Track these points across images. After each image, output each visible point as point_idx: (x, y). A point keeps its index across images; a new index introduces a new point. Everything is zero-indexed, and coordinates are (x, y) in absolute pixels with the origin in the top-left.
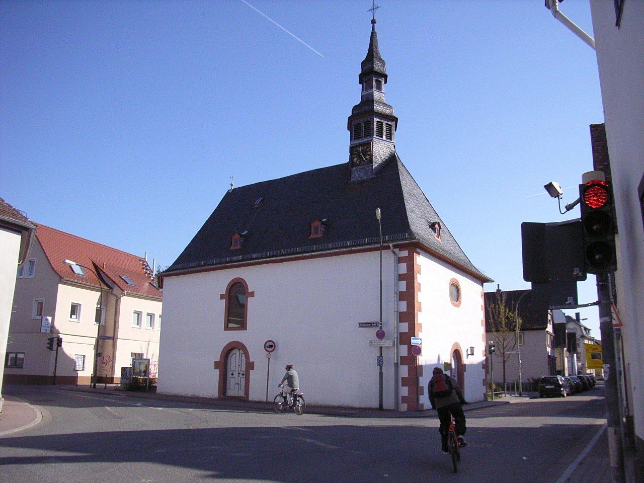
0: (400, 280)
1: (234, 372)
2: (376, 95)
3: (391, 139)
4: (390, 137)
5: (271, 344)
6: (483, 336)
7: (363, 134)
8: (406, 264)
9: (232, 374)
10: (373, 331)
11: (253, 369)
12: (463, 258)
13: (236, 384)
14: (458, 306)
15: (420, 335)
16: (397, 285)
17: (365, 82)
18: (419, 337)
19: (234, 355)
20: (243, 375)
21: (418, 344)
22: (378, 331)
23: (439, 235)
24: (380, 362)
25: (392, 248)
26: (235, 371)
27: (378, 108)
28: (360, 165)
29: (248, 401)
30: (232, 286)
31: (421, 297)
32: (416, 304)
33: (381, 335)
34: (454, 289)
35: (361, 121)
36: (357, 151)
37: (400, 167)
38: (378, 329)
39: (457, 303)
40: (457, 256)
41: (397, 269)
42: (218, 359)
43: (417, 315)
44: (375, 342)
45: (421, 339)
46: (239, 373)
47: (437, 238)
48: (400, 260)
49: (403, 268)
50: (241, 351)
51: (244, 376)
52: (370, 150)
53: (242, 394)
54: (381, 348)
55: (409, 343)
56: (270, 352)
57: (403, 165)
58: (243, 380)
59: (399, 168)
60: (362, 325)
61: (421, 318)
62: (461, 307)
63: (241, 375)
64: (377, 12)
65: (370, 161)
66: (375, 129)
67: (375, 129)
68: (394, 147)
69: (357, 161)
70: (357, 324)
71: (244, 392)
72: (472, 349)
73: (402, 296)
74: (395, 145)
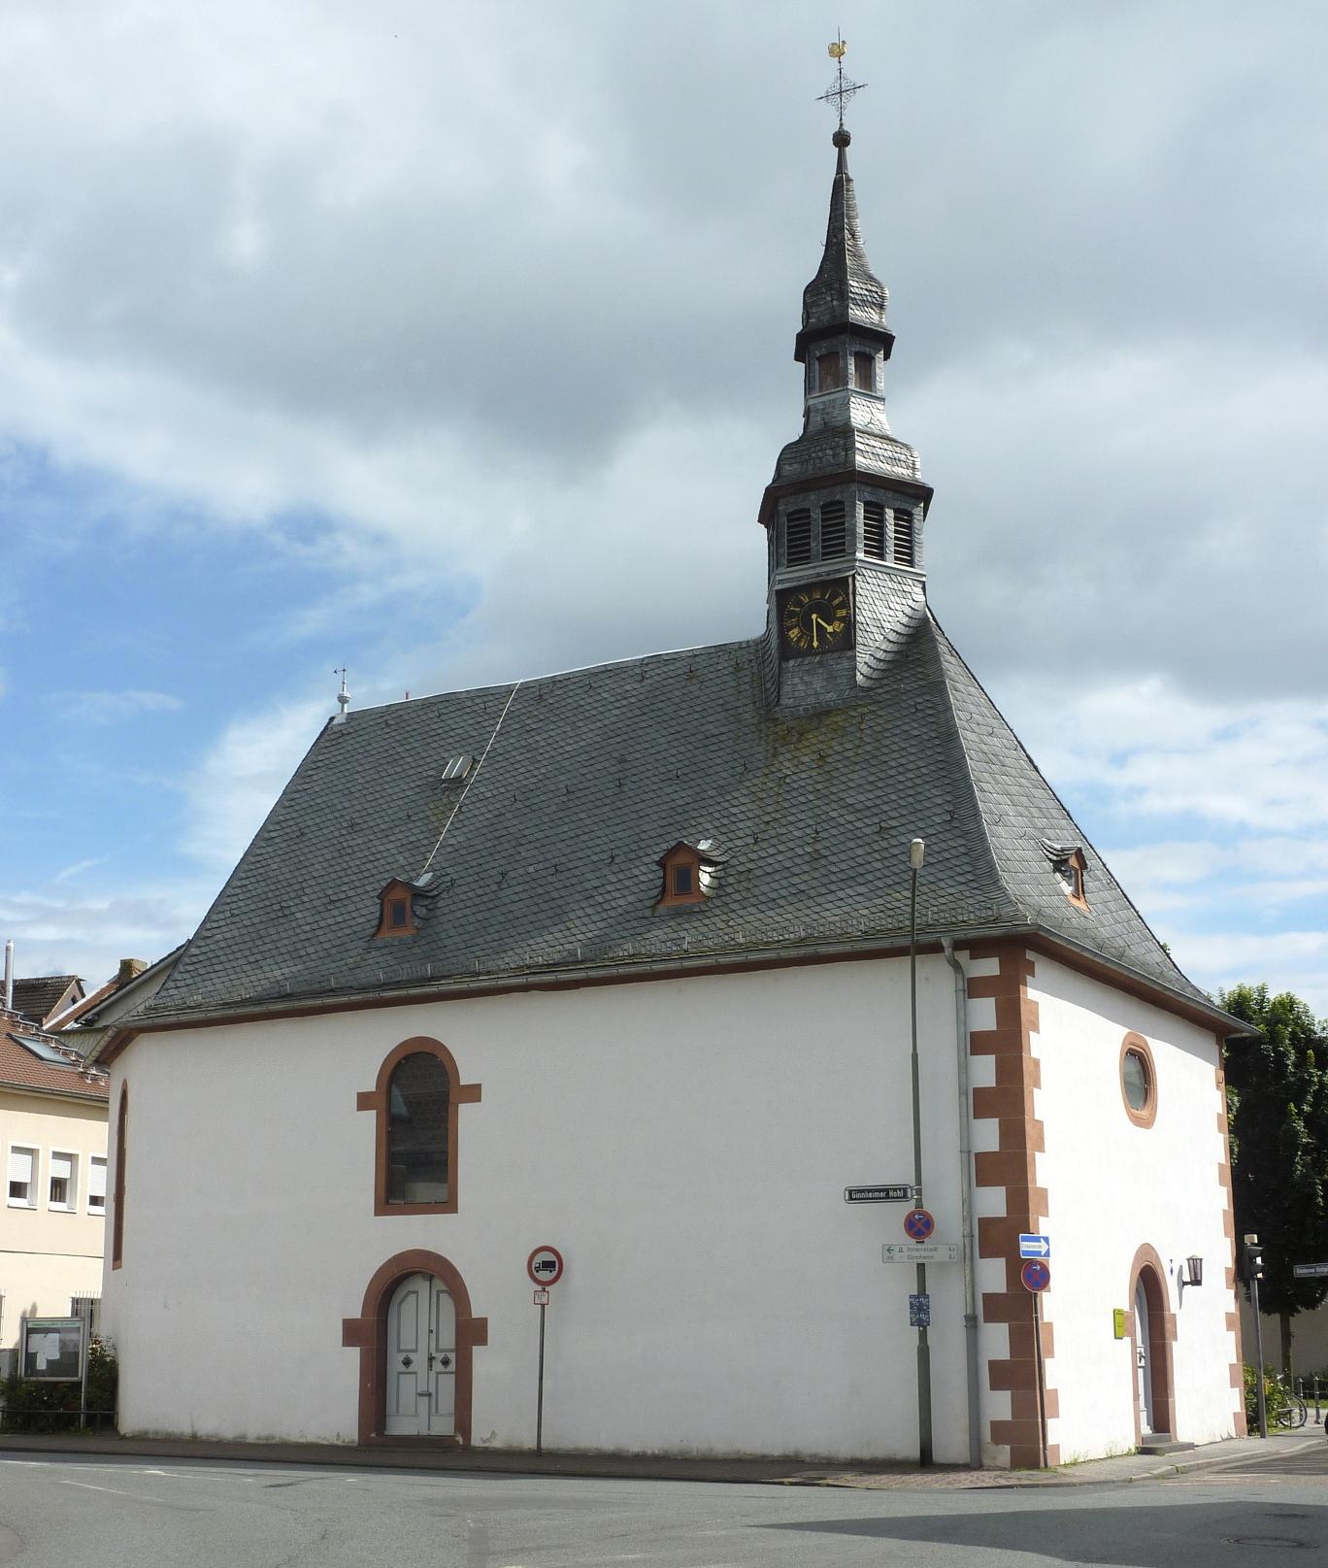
0: (975, 1051)
1: (412, 1356)
2: (860, 413)
3: (911, 563)
4: (907, 552)
5: (550, 1257)
6: (1041, 1138)
7: (816, 546)
8: (993, 999)
9: (407, 1362)
10: (897, 1213)
11: (482, 1340)
12: (1157, 956)
13: (421, 1395)
14: (1146, 1123)
15: (1044, 1226)
16: (964, 1069)
17: (818, 358)
18: (1042, 1233)
19: (412, 1297)
20: (446, 1362)
21: (1038, 1253)
22: (912, 1214)
23: (1080, 891)
24: (920, 1310)
25: (948, 951)
26: (416, 1351)
27: (867, 458)
28: (810, 651)
29: (468, 1449)
30: (399, 1064)
31: (1045, 1104)
32: (1028, 1128)
33: (919, 1226)
34: (1134, 1067)
35: (813, 502)
36: (799, 604)
37: (950, 665)
38: (909, 1207)
39: (1144, 1113)
40: (1140, 957)
41: (962, 1018)
42: (356, 1313)
43: (1034, 1160)
44: (901, 1251)
45: (1046, 1240)
46: (431, 1359)
47: (1075, 902)
48: (974, 988)
49: (984, 1014)
50: (439, 1284)
51: (452, 1367)
52: (845, 605)
53: (443, 1425)
54: (921, 1268)
55: (1012, 1253)
56: (544, 1284)
57: (953, 651)
58: (448, 1384)
59: (945, 665)
60: (856, 1195)
61: (1046, 1170)
62: (1154, 1127)
63: (438, 1366)
64: (854, 104)
65: (847, 641)
66: (861, 529)
67: (861, 529)
68: (924, 589)
69: (799, 640)
70: (841, 1195)
71: (452, 1420)
72: (1195, 1265)
73: (983, 1103)
74: (923, 583)
